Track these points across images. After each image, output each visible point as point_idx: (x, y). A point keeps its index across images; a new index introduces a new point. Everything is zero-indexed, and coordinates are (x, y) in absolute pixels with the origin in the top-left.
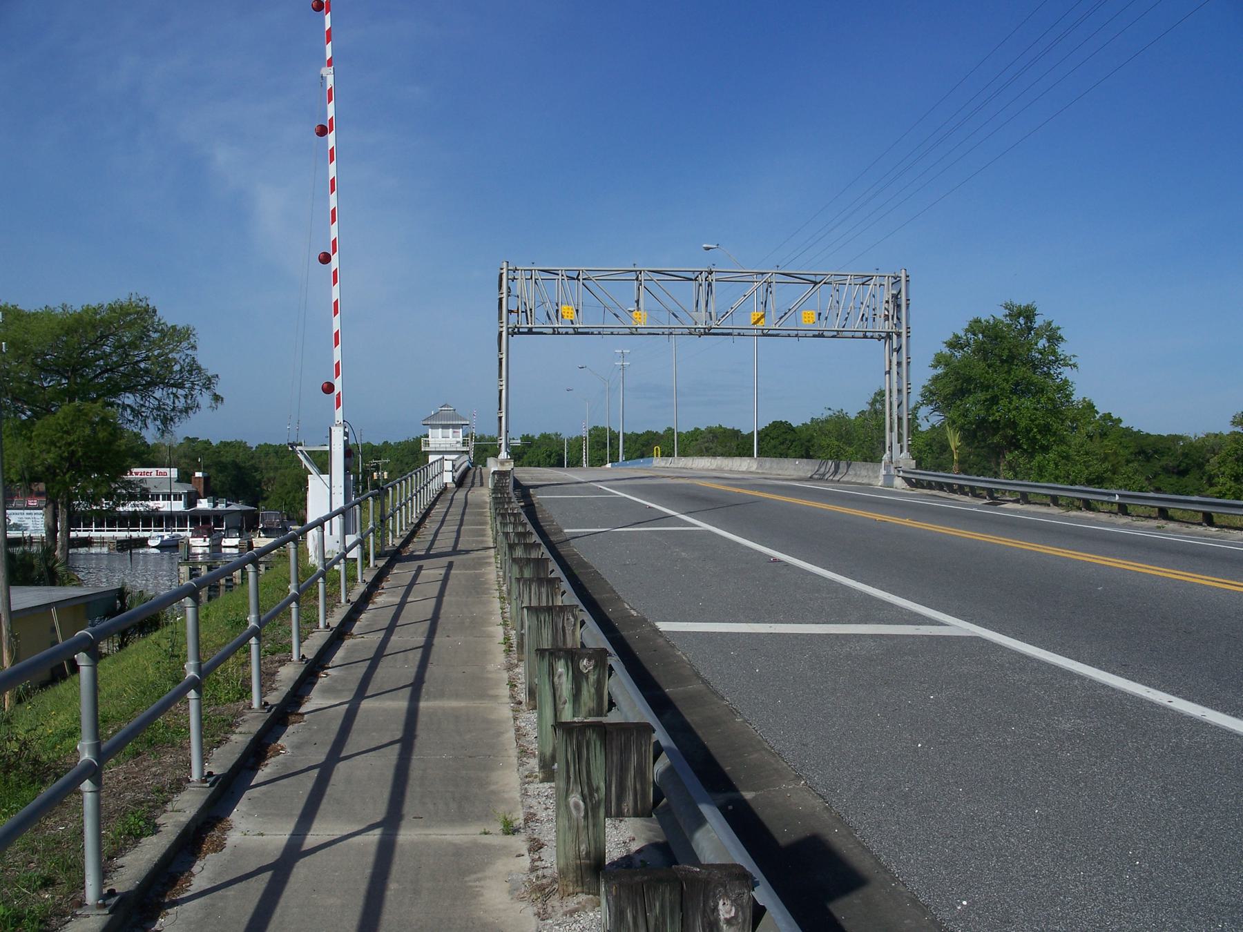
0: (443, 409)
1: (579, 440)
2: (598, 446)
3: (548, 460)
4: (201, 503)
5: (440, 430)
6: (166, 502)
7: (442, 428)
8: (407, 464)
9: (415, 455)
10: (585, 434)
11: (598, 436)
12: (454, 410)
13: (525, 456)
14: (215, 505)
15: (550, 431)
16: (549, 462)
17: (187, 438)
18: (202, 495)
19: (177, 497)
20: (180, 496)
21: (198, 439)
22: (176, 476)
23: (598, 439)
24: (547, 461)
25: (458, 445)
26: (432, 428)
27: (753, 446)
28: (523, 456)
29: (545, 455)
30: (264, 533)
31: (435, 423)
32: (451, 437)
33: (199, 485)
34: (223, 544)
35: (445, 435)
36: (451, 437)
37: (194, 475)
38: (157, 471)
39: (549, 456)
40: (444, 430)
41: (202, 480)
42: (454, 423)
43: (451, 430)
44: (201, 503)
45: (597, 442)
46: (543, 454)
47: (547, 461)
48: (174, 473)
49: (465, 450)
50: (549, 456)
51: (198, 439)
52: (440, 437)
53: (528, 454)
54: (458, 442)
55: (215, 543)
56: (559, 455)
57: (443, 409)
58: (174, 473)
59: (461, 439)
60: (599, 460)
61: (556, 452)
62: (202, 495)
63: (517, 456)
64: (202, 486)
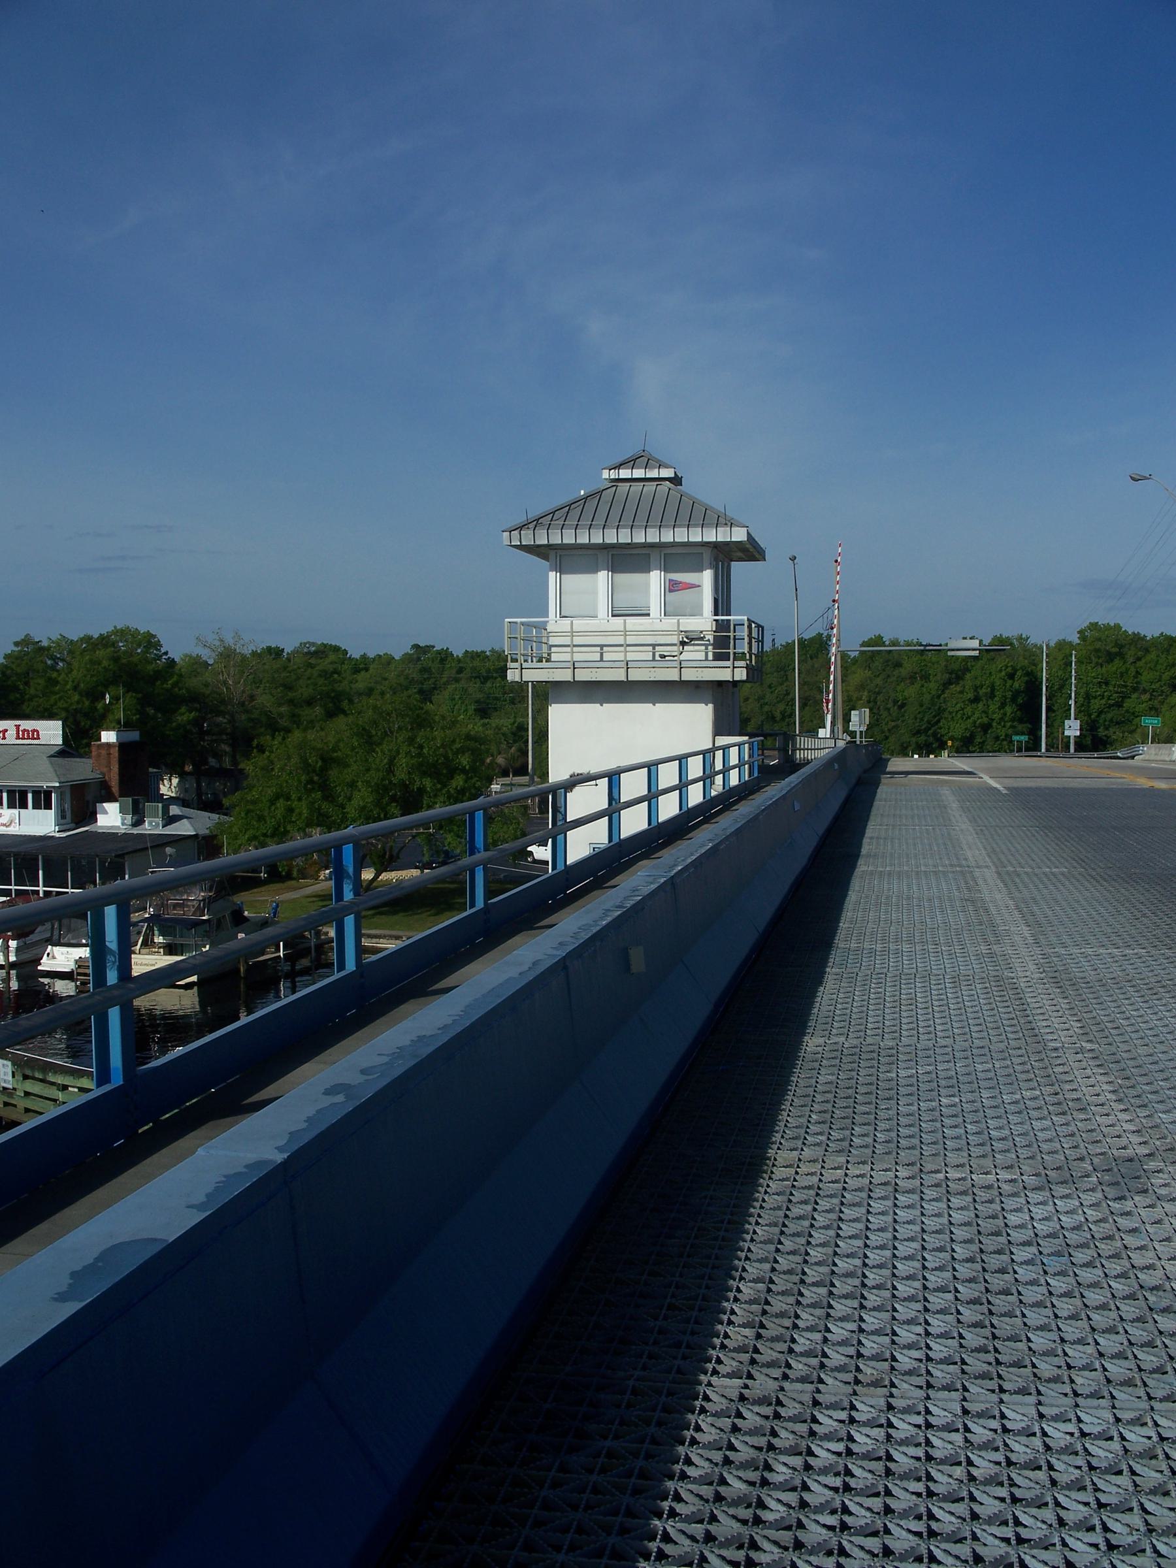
0: (625, 473)
1: (1062, 645)
2: (1099, 657)
3: (1010, 682)
4: (105, 812)
5: (603, 577)
6: (15, 812)
7: (614, 568)
8: (770, 687)
9: (782, 673)
10: (1075, 639)
11: (1099, 639)
12: (676, 480)
13: (968, 676)
14: (138, 823)
15: (1009, 632)
16: (1011, 686)
17: (416, 647)
18: (115, 789)
19: (43, 800)
20: (48, 794)
21: (434, 647)
22: (61, 742)
23: (1098, 645)
24: (1008, 685)
25: (694, 653)
26: (561, 570)
27: (794, 652)
28: (964, 674)
29: (1003, 673)
30: (162, 934)
31: (569, 539)
32: (655, 608)
33: (109, 765)
34: (46, 964)
35: (623, 602)
36: (655, 608)
37: (100, 739)
38: (18, 727)
39: (1011, 676)
40: (623, 578)
41: (115, 752)
42: (668, 536)
43: (656, 579)
44: (105, 812)
45: (1097, 651)
46: (1001, 671)
47: (1008, 685)
48: (51, 732)
49: (724, 675)
50: (1011, 676)
51: (434, 647)
52: (603, 608)
53: (973, 672)
54: (689, 639)
55: (26, 956)
56: (1028, 674)
57: (625, 473)
58: (51, 732)
59: (704, 622)
60: (1100, 682)
61: (1023, 668)
62: (115, 789)
63: (954, 676)
64: (115, 768)
